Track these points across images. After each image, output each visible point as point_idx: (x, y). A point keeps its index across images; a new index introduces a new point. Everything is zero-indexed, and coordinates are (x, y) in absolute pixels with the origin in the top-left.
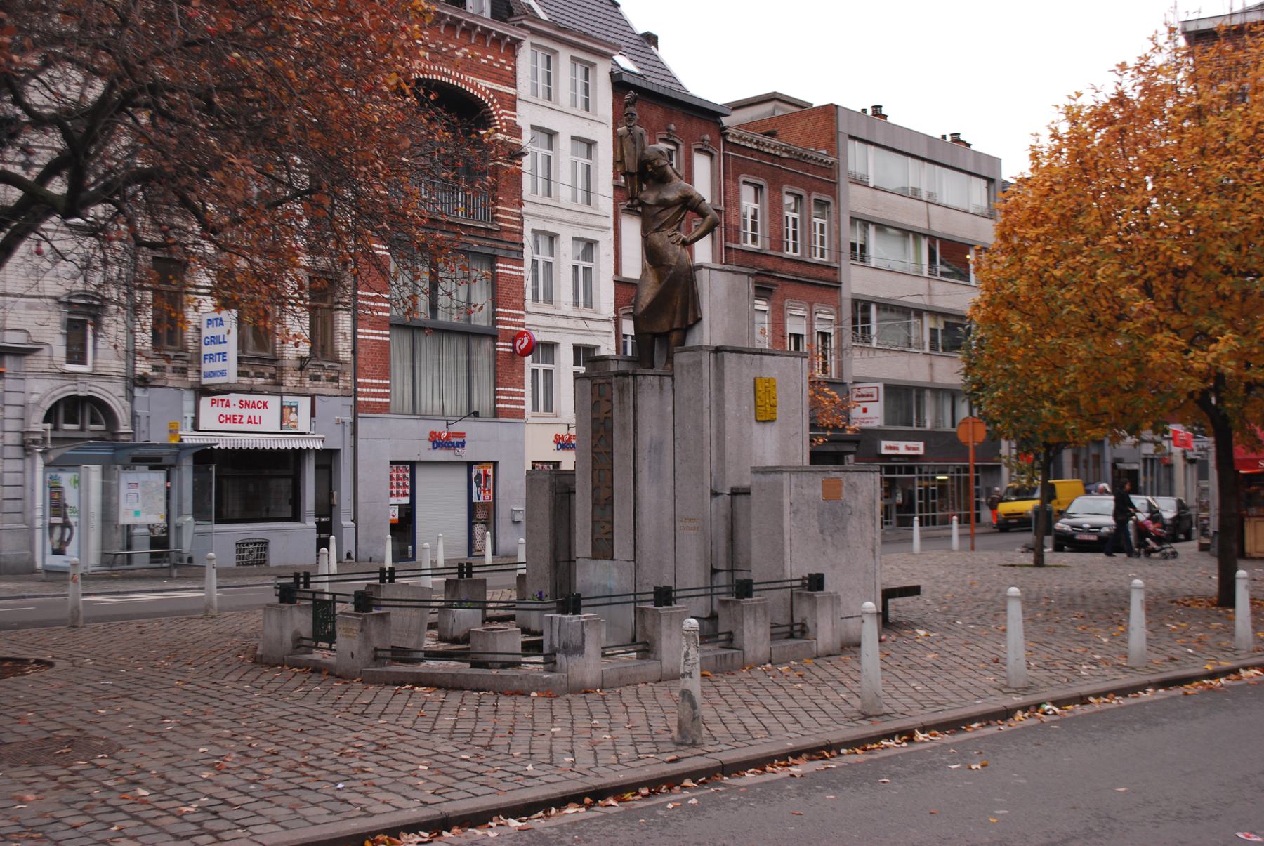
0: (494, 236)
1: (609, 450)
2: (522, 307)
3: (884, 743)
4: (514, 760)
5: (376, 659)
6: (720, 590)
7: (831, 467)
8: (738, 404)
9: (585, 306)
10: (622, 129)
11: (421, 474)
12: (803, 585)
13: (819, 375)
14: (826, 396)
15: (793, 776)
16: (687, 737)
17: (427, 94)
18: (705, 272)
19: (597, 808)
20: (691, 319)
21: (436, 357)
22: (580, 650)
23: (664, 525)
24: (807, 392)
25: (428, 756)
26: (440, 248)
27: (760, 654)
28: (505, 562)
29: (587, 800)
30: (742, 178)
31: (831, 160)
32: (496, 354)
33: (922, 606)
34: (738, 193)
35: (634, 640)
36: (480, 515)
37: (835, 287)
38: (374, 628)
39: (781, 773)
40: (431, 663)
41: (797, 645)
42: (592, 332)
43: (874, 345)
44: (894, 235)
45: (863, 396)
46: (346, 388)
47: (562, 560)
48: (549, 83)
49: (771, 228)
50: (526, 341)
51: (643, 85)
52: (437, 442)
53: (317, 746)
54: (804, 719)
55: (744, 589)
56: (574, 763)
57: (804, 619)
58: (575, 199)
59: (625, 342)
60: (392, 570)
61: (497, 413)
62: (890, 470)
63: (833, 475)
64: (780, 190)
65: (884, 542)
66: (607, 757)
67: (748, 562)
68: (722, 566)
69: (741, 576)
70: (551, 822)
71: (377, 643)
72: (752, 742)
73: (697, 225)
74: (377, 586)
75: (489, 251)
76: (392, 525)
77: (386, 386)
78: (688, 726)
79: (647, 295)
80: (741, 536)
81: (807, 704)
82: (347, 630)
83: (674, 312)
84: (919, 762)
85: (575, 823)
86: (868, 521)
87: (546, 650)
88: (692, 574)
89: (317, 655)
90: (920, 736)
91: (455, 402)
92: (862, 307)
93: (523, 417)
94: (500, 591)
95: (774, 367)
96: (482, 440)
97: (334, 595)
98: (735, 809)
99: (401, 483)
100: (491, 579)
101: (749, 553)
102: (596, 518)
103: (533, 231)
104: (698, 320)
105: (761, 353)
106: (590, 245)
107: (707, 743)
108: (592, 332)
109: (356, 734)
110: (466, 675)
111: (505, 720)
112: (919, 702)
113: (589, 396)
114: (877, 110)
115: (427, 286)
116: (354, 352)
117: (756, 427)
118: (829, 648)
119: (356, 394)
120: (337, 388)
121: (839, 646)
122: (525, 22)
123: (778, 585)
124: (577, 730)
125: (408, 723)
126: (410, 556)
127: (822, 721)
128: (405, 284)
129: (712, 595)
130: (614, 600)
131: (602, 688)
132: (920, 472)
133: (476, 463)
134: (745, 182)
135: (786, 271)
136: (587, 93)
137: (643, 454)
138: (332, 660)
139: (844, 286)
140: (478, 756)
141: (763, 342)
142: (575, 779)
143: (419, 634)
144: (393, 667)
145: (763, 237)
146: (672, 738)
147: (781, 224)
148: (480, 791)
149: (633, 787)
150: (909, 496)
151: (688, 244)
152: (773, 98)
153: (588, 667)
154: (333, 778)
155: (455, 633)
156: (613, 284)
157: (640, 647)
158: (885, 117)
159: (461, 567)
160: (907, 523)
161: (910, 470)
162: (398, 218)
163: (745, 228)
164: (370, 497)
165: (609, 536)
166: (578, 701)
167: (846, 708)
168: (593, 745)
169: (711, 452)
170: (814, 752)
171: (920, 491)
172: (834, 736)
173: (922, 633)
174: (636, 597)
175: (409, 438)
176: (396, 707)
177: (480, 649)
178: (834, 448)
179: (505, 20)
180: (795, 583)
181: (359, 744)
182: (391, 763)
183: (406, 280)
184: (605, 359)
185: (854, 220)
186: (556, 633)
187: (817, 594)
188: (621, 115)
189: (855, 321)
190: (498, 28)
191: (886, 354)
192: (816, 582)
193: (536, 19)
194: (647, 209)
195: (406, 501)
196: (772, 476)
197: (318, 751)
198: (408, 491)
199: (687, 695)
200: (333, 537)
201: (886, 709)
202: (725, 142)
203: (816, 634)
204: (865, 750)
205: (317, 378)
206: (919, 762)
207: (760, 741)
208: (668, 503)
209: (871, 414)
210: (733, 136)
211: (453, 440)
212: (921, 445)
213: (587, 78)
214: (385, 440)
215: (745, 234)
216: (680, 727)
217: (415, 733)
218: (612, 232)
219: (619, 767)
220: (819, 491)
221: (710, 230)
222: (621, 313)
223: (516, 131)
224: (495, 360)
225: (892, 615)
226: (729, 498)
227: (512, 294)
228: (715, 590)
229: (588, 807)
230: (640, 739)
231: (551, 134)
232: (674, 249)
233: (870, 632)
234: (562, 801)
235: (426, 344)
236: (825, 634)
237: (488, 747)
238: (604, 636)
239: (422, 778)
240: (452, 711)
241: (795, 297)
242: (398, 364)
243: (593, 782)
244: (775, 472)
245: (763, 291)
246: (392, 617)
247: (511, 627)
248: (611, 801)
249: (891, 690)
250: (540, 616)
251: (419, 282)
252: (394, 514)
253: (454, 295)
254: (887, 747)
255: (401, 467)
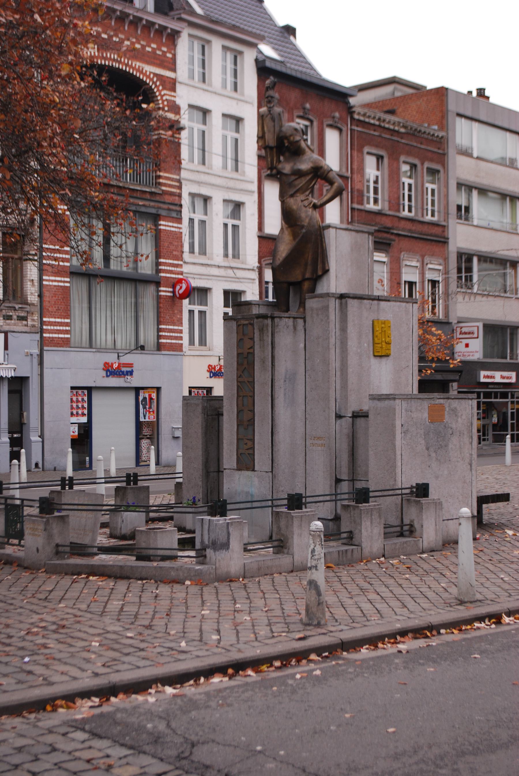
0: (158, 198)
1: (251, 380)
2: (180, 258)
3: (477, 625)
4: (171, 638)
5: (57, 553)
6: (343, 497)
7: (436, 395)
8: (358, 342)
9: (234, 256)
10: (264, 109)
11: (96, 398)
12: (412, 493)
13: (428, 316)
14: (434, 335)
15: (400, 652)
16: (313, 619)
17: (100, 75)
18: (332, 231)
19: (238, 678)
20: (320, 268)
21: (109, 299)
22: (226, 546)
23: (297, 443)
24: (417, 332)
25: (99, 635)
26: (114, 207)
27: (375, 550)
28: (166, 470)
29: (230, 671)
30: (366, 149)
31: (441, 134)
32: (159, 297)
33: (511, 510)
34: (362, 162)
35: (271, 537)
36: (146, 431)
37: (443, 241)
38: (55, 528)
39: (389, 649)
40: (103, 556)
41: (406, 542)
42: (238, 279)
43: (475, 290)
44: (494, 199)
45: (465, 333)
46: (33, 326)
47: (212, 470)
48: (204, 67)
49: (390, 192)
50: (184, 286)
51: (283, 70)
52: (111, 371)
53: (7, 626)
54: (411, 604)
55: (363, 496)
56: (219, 641)
57: (412, 521)
58: (225, 167)
59: (267, 288)
60: (71, 479)
61: (159, 347)
62: (487, 395)
63: (438, 401)
64: (397, 160)
65: (479, 456)
66: (247, 635)
67: (366, 473)
68: (344, 477)
69: (359, 485)
70: (200, 689)
71: (58, 540)
72: (367, 623)
73: (327, 190)
74: (59, 492)
75: (153, 211)
76: (72, 440)
77: (67, 324)
78: (314, 610)
79: (284, 250)
80: (360, 452)
81: (413, 591)
82: (33, 529)
83: (306, 265)
84: (505, 641)
85: (220, 691)
86: (466, 440)
87: (198, 546)
88: (319, 483)
89: (9, 550)
90: (506, 619)
91: (124, 338)
92: (465, 259)
93: (181, 350)
94: (161, 496)
95: (389, 311)
96: (147, 370)
97: (22, 500)
98: (352, 679)
99: (80, 405)
100: (153, 485)
101: (367, 466)
102: (240, 437)
103: (190, 194)
104: (326, 271)
105: (379, 299)
106: (238, 206)
107: (329, 624)
108: (238, 279)
109: (41, 616)
110: (132, 567)
111: (164, 604)
112: (506, 591)
113: (235, 335)
114: (481, 92)
115: (101, 239)
116: (40, 296)
117: (374, 361)
118: (433, 545)
119: (42, 331)
120: (26, 325)
121: (441, 543)
122: (184, 16)
123: (391, 493)
124: (222, 613)
125: (84, 607)
126: (88, 465)
127: (426, 606)
128: (82, 239)
129: (336, 501)
130: (255, 505)
131: (244, 577)
132: (513, 397)
133: (143, 388)
134: (368, 153)
135: (402, 229)
136: (235, 76)
137: (279, 383)
138: (21, 554)
139: (451, 241)
140: (140, 634)
141: (381, 289)
142: (220, 653)
143: (94, 532)
144: (72, 559)
145: (383, 200)
146: (301, 620)
147: (399, 188)
148: (141, 663)
149: (268, 660)
150: (503, 417)
151: (319, 207)
152: (393, 81)
153: (233, 560)
154: (21, 653)
155: (124, 532)
156: (257, 240)
157: (276, 544)
158: (488, 98)
159: (128, 476)
160: (500, 439)
161: (504, 395)
162: (79, 181)
163: (368, 191)
164: (55, 417)
165: (251, 451)
166: (224, 588)
167: (445, 595)
168: (236, 625)
169: (336, 382)
170: (418, 632)
171: (512, 413)
172: (435, 618)
173: (510, 532)
174: (273, 502)
175: (86, 367)
176: (73, 594)
177: (143, 545)
178: (438, 378)
179: (166, 14)
180: (404, 491)
181: (43, 624)
182: (69, 640)
183: (84, 236)
184: (249, 304)
185: (460, 185)
186: (206, 532)
187: (423, 500)
188: (264, 98)
189: (459, 271)
190: (160, 21)
191: (484, 299)
192: (422, 490)
193: (193, 13)
194: (284, 178)
195: (84, 420)
196: (387, 402)
197: (8, 630)
198: (86, 412)
199: (313, 584)
200: (23, 451)
201: (479, 597)
202: (352, 118)
203: (422, 534)
204: (460, 630)
205: (10, 318)
206: (505, 641)
207: (373, 623)
208: (300, 425)
209: (471, 349)
210: (359, 114)
211: (123, 369)
212: (513, 374)
213: (235, 64)
214: (66, 371)
215: (368, 198)
216: (307, 610)
217: (89, 615)
218: (256, 195)
219: (256, 644)
220: (426, 415)
221: (339, 193)
222: (264, 263)
223: (175, 109)
224: (158, 303)
225: (485, 518)
226: (351, 420)
227: (172, 247)
228: (339, 497)
229: (231, 677)
230: (274, 620)
231: (205, 112)
232: (306, 212)
233: (465, 532)
234: (209, 672)
235: (101, 289)
236: (430, 533)
237: (149, 627)
238: (246, 534)
239: (94, 653)
240: (120, 596)
241: (409, 250)
242: (77, 305)
243: (235, 656)
244: (389, 399)
245: (381, 245)
246: (71, 519)
247: (169, 527)
248: (250, 672)
249: (483, 580)
250: (194, 518)
251: (95, 237)
252: (75, 431)
253: (124, 247)
254: (478, 628)
255: (80, 392)
